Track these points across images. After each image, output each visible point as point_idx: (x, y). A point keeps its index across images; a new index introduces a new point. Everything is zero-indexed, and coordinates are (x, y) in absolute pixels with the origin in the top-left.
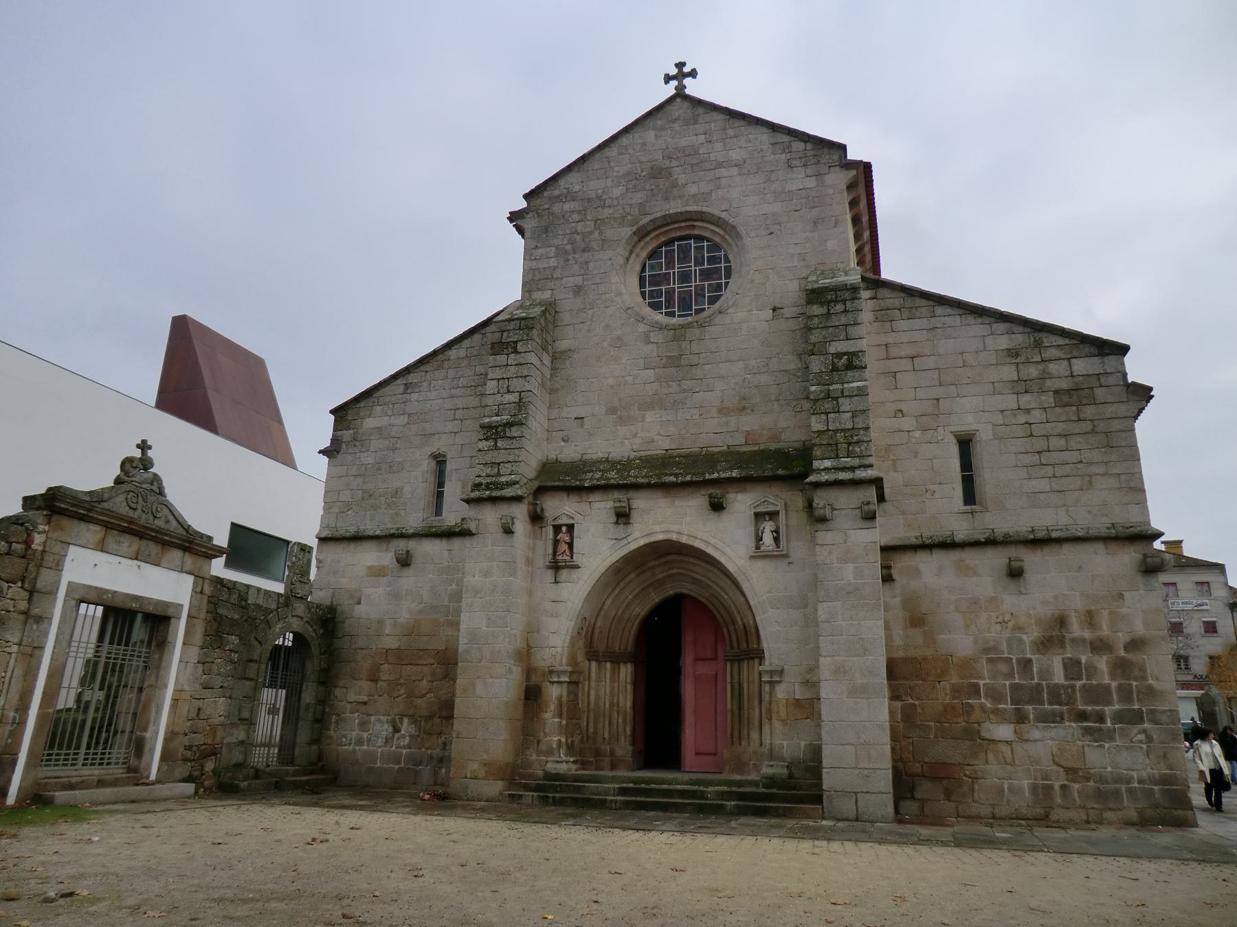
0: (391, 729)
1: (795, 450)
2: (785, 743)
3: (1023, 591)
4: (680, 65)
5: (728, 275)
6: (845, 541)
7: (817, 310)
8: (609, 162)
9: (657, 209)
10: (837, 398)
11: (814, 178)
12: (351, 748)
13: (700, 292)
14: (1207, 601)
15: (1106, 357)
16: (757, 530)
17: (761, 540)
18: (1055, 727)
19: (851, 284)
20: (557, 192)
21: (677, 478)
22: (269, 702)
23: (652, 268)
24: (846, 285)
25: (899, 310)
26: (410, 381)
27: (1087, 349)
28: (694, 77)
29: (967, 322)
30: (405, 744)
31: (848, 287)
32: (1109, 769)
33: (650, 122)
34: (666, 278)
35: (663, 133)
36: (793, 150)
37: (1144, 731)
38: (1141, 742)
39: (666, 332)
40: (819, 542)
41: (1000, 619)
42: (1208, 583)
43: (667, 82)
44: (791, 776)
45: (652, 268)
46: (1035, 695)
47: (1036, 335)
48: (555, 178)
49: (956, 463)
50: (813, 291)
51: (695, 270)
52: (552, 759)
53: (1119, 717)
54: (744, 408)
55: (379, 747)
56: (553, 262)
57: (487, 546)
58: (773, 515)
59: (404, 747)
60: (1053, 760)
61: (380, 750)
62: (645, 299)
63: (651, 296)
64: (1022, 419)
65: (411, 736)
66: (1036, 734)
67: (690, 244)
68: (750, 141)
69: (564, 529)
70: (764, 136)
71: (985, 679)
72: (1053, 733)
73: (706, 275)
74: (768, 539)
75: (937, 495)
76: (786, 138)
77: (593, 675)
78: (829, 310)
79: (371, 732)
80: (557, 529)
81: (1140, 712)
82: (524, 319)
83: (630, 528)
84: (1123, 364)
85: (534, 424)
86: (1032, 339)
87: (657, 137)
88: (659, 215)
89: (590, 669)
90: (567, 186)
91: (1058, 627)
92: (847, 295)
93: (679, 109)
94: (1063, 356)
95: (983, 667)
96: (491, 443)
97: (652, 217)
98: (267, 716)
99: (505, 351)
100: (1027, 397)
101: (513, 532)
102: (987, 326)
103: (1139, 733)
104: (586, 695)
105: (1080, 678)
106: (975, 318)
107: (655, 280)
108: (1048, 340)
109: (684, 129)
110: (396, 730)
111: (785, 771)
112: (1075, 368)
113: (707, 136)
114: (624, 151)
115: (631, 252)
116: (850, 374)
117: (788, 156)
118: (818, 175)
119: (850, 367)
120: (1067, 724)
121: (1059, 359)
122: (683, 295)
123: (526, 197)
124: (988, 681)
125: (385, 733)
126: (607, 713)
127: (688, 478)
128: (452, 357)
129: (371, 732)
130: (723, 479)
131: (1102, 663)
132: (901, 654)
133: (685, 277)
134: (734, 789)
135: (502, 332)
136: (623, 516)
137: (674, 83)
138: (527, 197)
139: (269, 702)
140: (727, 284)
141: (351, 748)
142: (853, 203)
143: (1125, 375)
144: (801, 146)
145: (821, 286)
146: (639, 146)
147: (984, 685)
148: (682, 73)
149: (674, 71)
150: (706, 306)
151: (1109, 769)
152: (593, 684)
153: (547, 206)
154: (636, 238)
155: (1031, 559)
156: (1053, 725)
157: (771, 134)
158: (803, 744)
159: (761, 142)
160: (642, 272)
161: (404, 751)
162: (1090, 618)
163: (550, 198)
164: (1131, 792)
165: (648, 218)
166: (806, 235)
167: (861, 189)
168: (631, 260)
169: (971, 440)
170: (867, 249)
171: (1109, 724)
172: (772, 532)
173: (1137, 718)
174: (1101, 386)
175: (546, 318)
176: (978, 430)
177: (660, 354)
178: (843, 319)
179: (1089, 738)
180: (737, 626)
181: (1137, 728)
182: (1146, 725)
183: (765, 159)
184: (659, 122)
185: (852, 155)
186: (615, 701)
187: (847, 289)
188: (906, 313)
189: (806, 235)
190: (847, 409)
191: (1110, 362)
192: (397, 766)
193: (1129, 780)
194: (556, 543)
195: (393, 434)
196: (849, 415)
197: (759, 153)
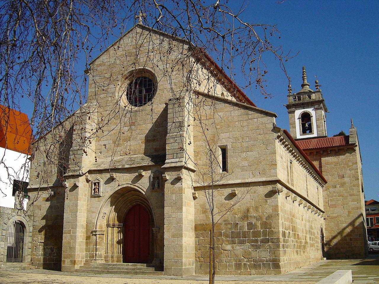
9: (144, 92)
12: (40, 257)
22: (12, 243)
32: (258, 258)
37: (269, 245)
46: (238, 235)
52: (94, 259)
53: (262, 241)
54: (154, 140)
61: (48, 257)
66: (238, 247)
69: (97, 184)
72: (243, 247)
74: (156, 186)
81: (269, 239)
90: (102, 60)
95: (223, 227)
120: (247, 244)
131: (259, 224)
132: (199, 223)
139: (12, 243)
141: (40, 257)
151: (258, 258)
155: (238, 191)
162: (256, 209)
169: (160, 267)
171: (259, 244)
173: (268, 241)
176: (227, 145)
182: (270, 243)
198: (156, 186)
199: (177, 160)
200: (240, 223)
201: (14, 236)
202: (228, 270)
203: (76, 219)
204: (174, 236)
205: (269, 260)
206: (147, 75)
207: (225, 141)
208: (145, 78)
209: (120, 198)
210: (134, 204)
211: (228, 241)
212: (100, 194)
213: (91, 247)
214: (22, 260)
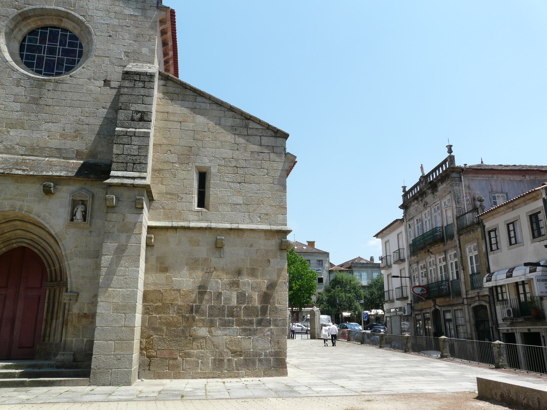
1: (105, 165)
2: (74, 339)
3: (222, 256)
6: (124, 220)
7: (127, 83)
10: (131, 136)
11: (140, 10)
13: (60, 62)
14: (321, 269)
16: (73, 209)
17: (75, 215)
19: (150, 73)
21: (428, 319)
23: (30, 40)
25: (177, 95)
27: (270, 133)
29: (213, 108)
34: (39, 49)
38: (268, 335)
42: (322, 261)
44: (74, 360)
45: (30, 40)
46: (221, 310)
51: (59, 48)
58: (83, 203)
60: (226, 346)
62: (22, 59)
63: (26, 59)
64: (234, 164)
66: (219, 332)
67: (58, 32)
72: (227, 332)
73: (66, 53)
74: (79, 215)
75: (183, 200)
78: (134, 85)
84: (285, 143)
86: (244, 123)
88: (38, 7)
92: (147, 79)
97: (34, 7)
100: (237, 152)
105: (244, 303)
107: (31, 49)
108: (252, 125)
112: (263, 142)
115: (15, 26)
116: (141, 123)
119: (141, 119)
121: (256, 135)
122: (49, 62)
124: (198, 304)
127: (31, 173)
132: (152, 288)
133: (52, 51)
143: (285, 149)
145: (132, 70)
150: (64, 72)
158: (85, 340)
164: (260, 360)
165: (31, 7)
166: (131, 42)
167: (168, 25)
168: (15, 32)
170: (171, 62)
172: (82, 212)
174: (274, 152)
177: (26, 94)
178: (142, 92)
182: (272, 327)
188: (181, 97)
189: (131, 42)
191: (280, 140)
196: (137, 147)
198: (79, 215)
199: (136, 174)
200: (226, 293)
202: (199, 371)
204: (117, 309)
207: (207, 161)
208: (65, 30)
213: (81, 338)
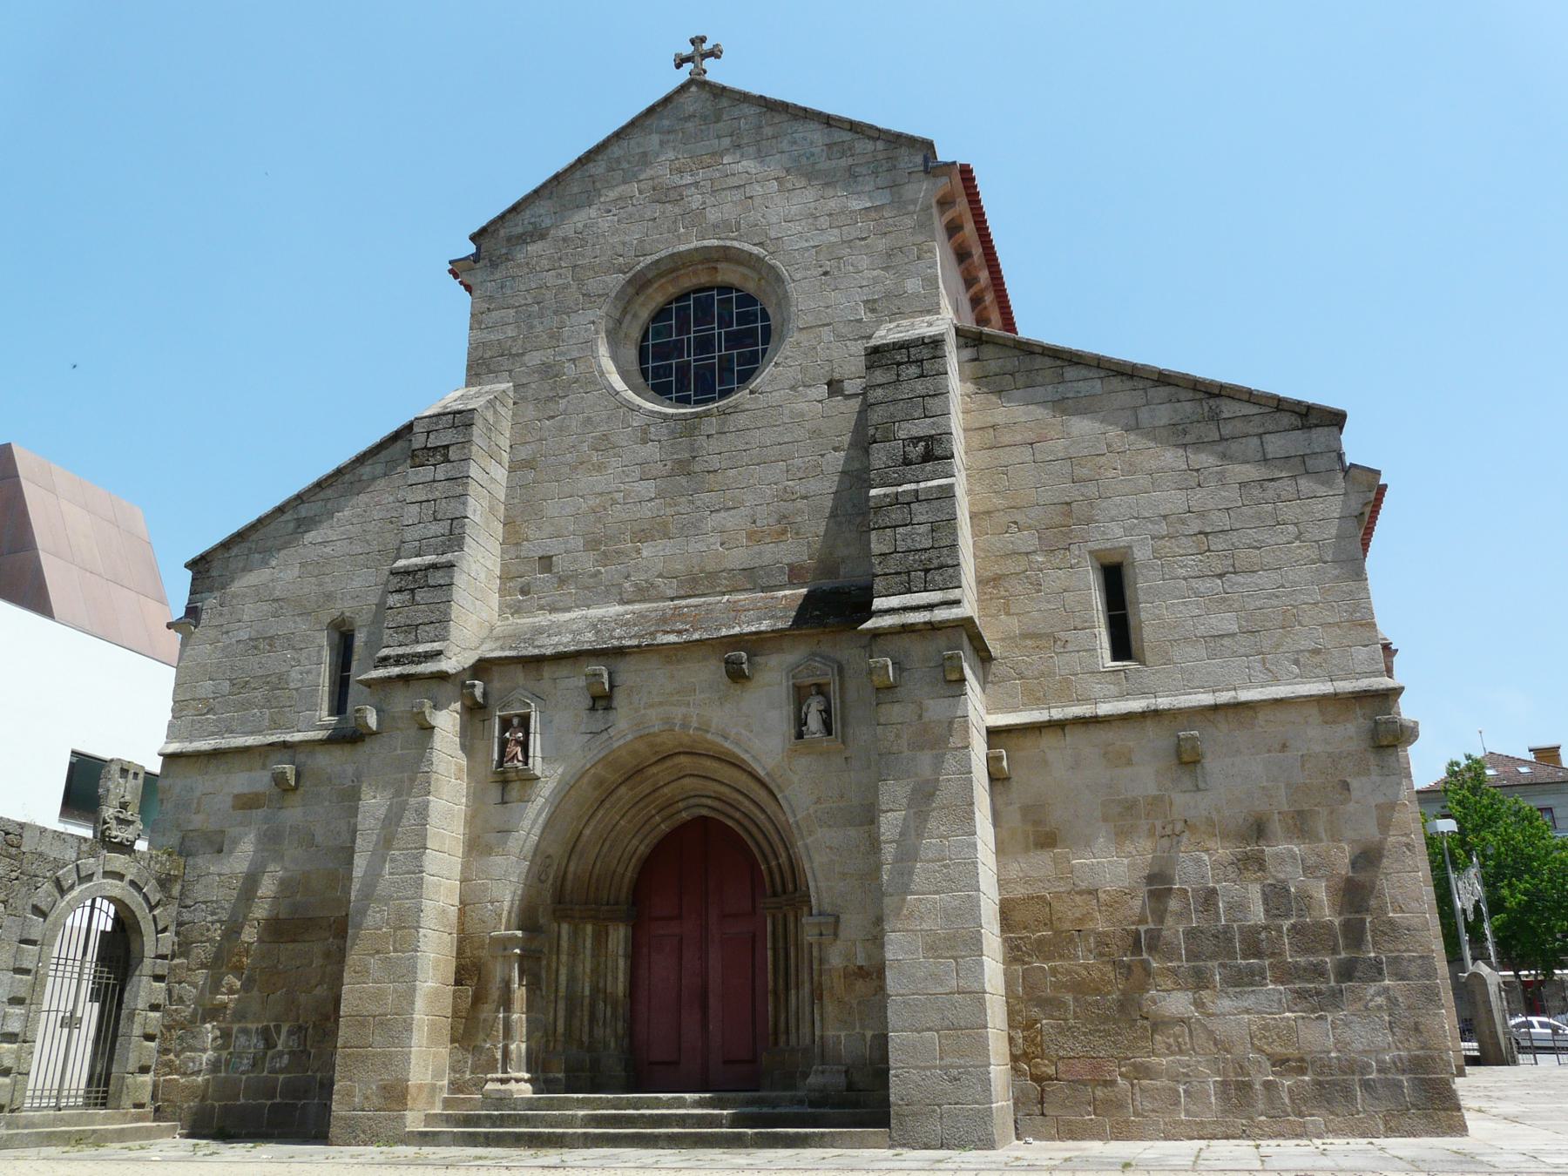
0: (261, 1045)
2: (843, 1034)
3: (1202, 785)
4: (698, 41)
5: (766, 341)
6: (920, 717)
7: (880, 376)
8: (594, 182)
15: (1314, 431)
17: (806, 724)
18: (1253, 991)
19: (930, 337)
20: (520, 230)
23: (657, 334)
24: (923, 338)
26: (303, 514)
27: (1286, 420)
28: (718, 57)
30: (283, 1066)
31: (926, 341)
33: (652, 122)
34: (677, 348)
35: (671, 137)
36: (857, 152)
38: (1380, 1007)
39: (672, 424)
40: (882, 720)
41: (1168, 831)
43: (678, 66)
44: (850, 1087)
45: (657, 334)
46: (1223, 937)
47: (1211, 402)
48: (515, 209)
49: (1097, 600)
50: (876, 350)
51: (720, 334)
52: (494, 1076)
55: (243, 1073)
56: (511, 332)
57: (395, 750)
58: (821, 690)
59: (282, 1071)
61: (244, 1077)
62: (647, 380)
63: (656, 375)
64: (1195, 526)
65: (292, 1053)
66: (1226, 1004)
67: (713, 296)
68: (795, 143)
70: (817, 136)
71: (1147, 923)
72: (1249, 1002)
73: (734, 340)
74: (814, 722)
75: (1070, 647)
76: (847, 136)
77: (564, 944)
78: (898, 375)
79: (231, 1050)
80: (506, 724)
82: (460, 412)
83: (612, 715)
85: (474, 567)
87: (662, 143)
88: (663, 254)
89: (559, 932)
90: (533, 220)
91: (1255, 837)
92: (926, 353)
93: (693, 102)
94: (1252, 431)
96: (406, 596)
97: (655, 257)
98: (58, 1029)
99: (432, 461)
100: (1200, 493)
101: (434, 728)
102: (1141, 392)
103: (1378, 994)
104: (553, 977)
105: (1287, 916)
106: (1122, 381)
109: (702, 131)
110: (269, 1044)
111: (841, 1080)
113: (734, 138)
114: (615, 166)
115: (625, 312)
116: (929, 466)
117: (850, 161)
118: (894, 186)
119: (928, 457)
123: (474, 238)
124: (1152, 926)
125: (252, 1050)
126: (587, 1001)
127: (696, 636)
128: (364, 477)
129: (231, 1050)
130: (747, 634)
131: (1321, 892)
132: (1020, 891)
134: (765, 1110)
135: (428, 433)
136: (602, 701)
137: (688, 66)
138: (474, 238)
140: (764, 351)
142: (953, 229)
143: (1340, 456)
144: (870, 146)
146: (637, 158)
147: (1146, 932)
148: (701, 51)
149: (688, 50)
152: (564, 958)
153: (504, 251)
154: (631, 291)
156: (1250, 989)
157: (826, 131)
159: (812, 143)
160: (642, 341)
161: (281, 1077)
163: (509, 239)
167: (962, 205)
170: (989, 298)
172: (820, 712)
174: (1307, 473)
175: (496, 412)
178: (920, 387)
179: (1305, 1005)
180: (780, 861)
181: (1372, 989)
182: (1387, 982)
183: (817, 167)
184: (666, 123)
185: (943, 155)
186: (601, 985)
187: (924, 343)
188: (1021, 380)
189: (875, 273)
190: (922, 519)
191: (1320, 436)
192: (269, 1102)
193: (1365, 1068)
194: (504, 744)
195: (277, 593)
197: (808, 158)
198: (814, 722)
200: (1228, 889)
201: (76, 975)
203: (419, 884)
205: (1395, 1063)
206: (728, 274)
207: (1119, 532)
208: (726, 289)
209: (623, 789)
210: (684, 814)
211: (1174, 972)
212: (531, 765)
214: (103, 1098)
